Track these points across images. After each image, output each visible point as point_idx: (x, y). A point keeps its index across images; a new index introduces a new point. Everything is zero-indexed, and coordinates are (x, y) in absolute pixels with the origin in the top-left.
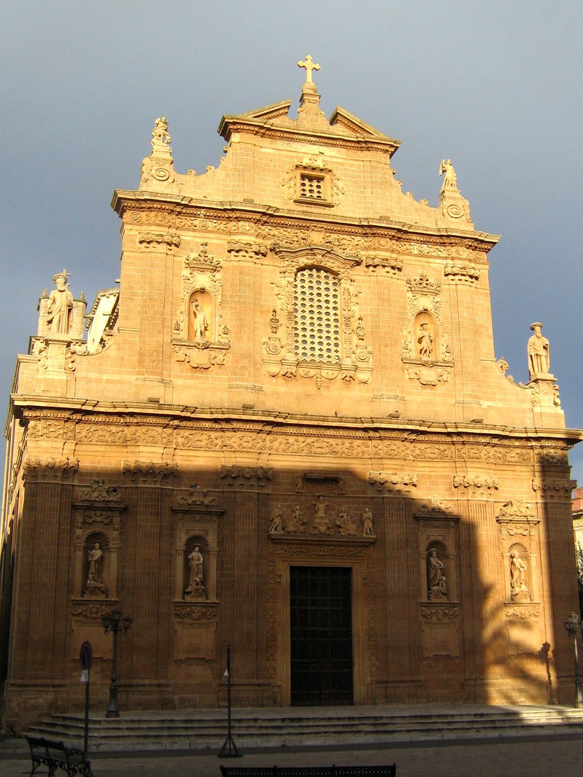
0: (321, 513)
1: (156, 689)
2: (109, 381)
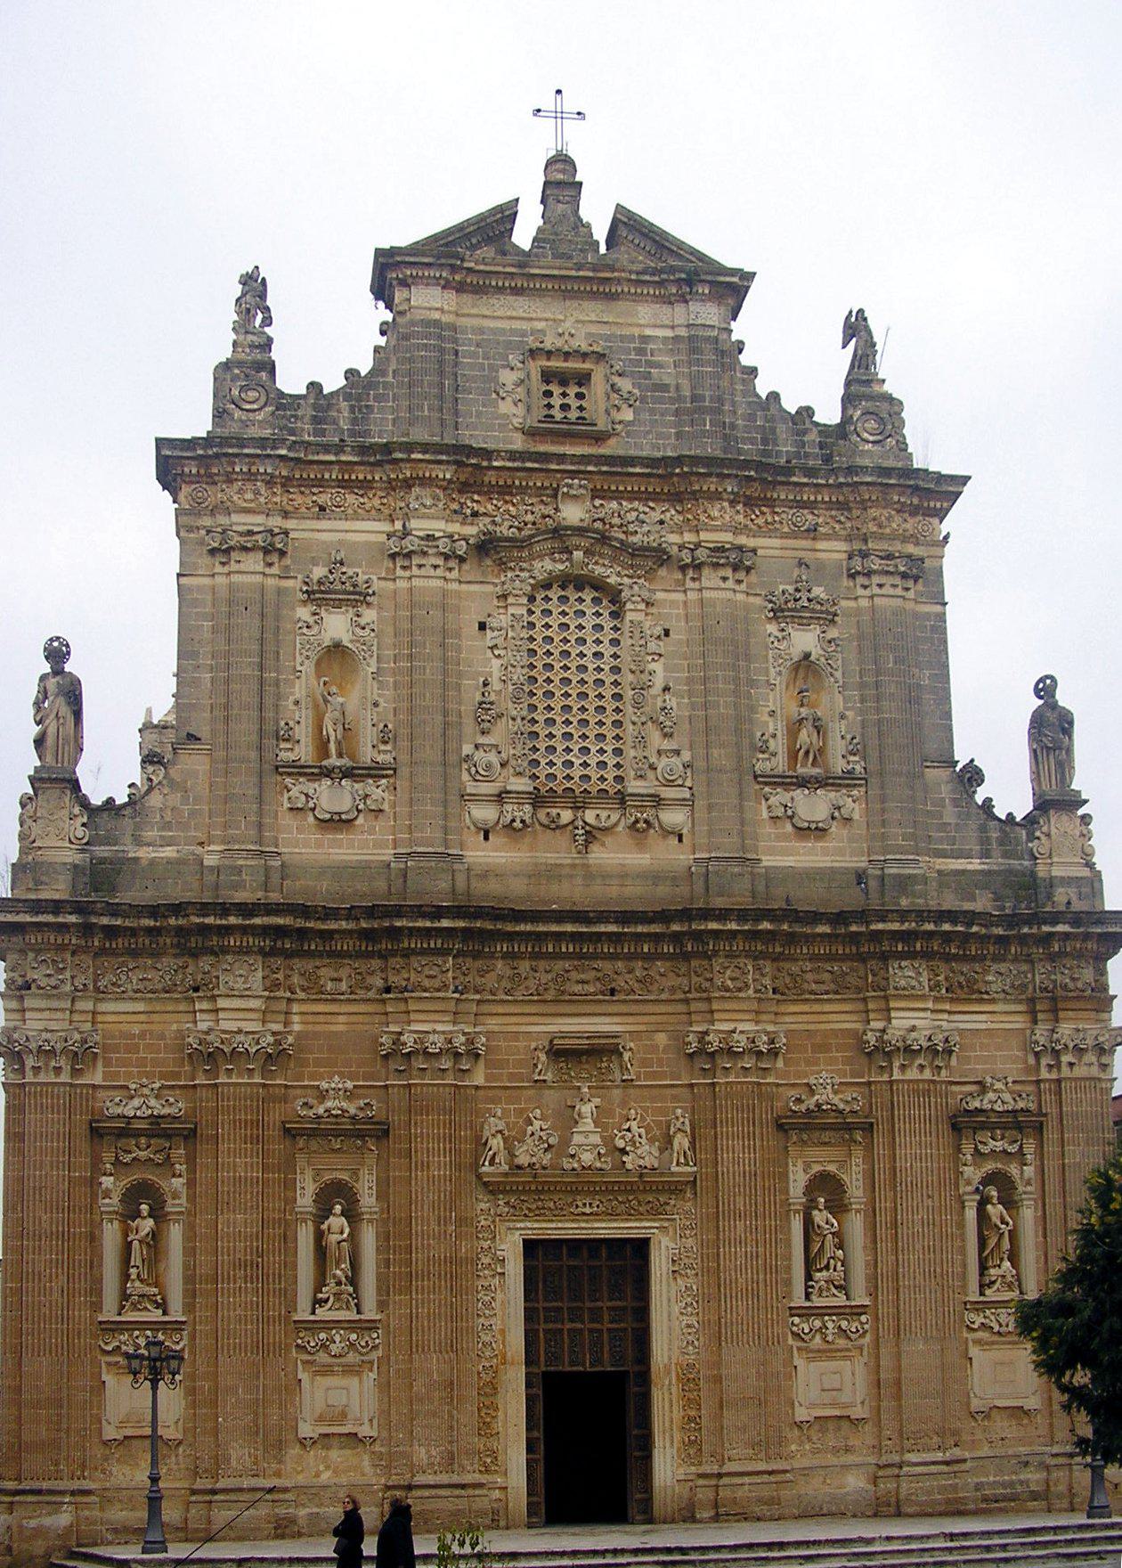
0: (588, 1124)
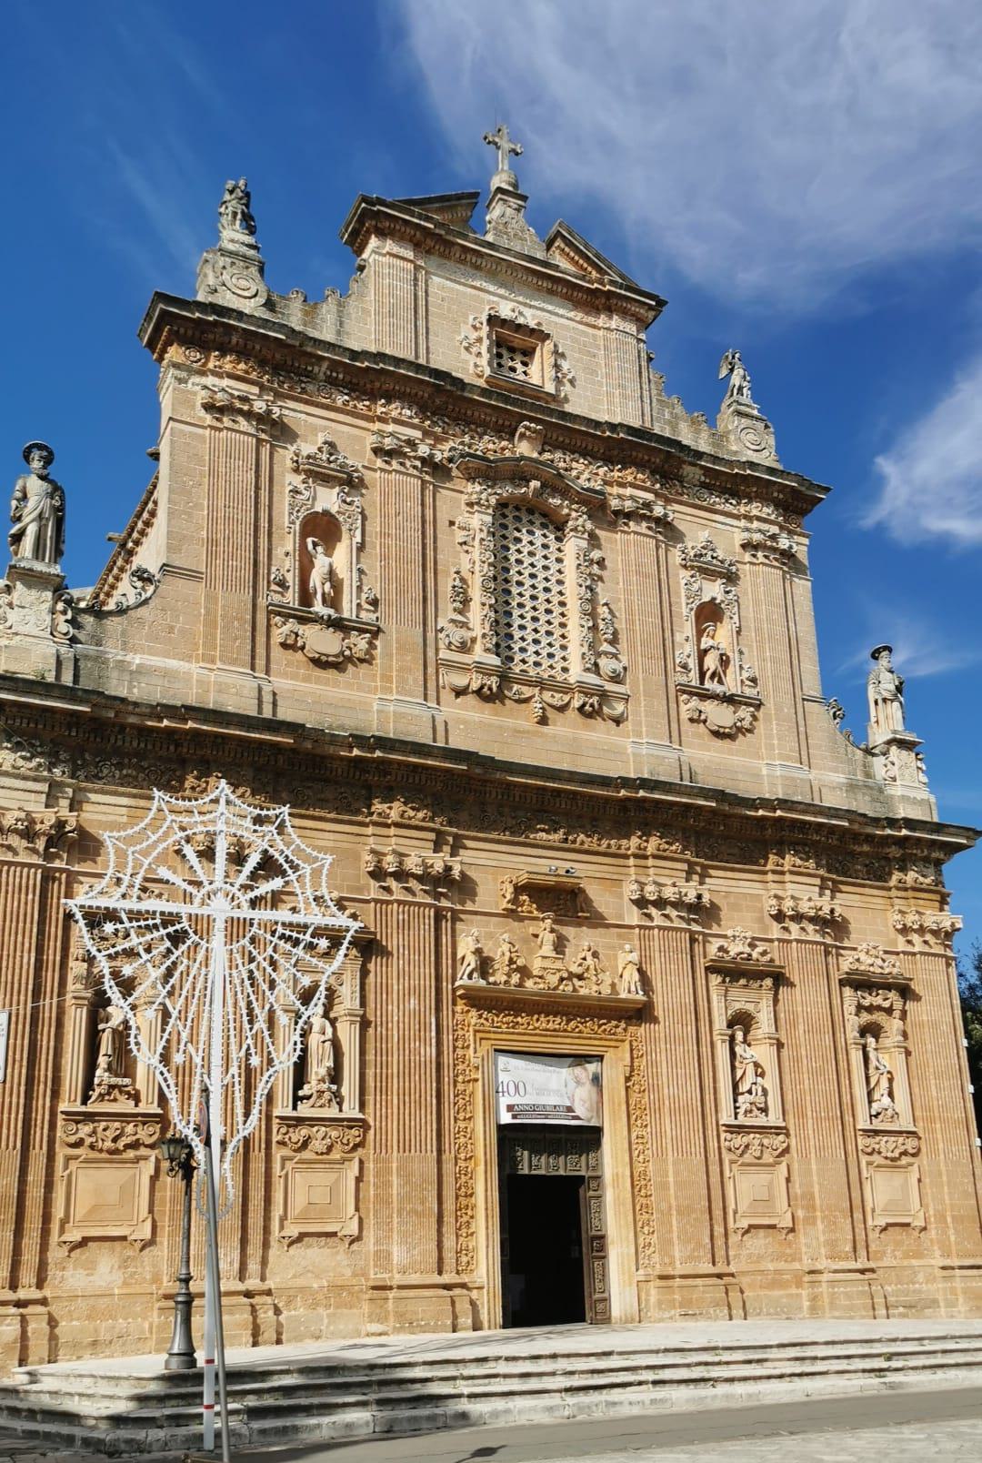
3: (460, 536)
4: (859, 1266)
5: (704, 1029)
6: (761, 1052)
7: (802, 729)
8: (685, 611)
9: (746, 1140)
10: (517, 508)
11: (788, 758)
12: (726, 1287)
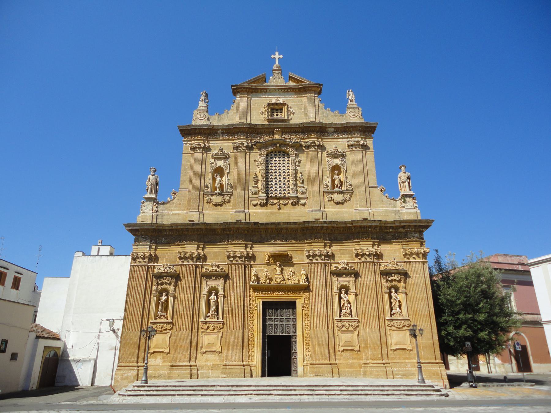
1: (382, 365)
2: (173, 215)
3: (257, 164)
4: (384, 362)
5: (329, 291)
6: (351, 298)
7: (368, 197)
8: (327, 169)
9: (343, 323)
10: (275, 152)
11: (363, 206)
12: (334, 369)
